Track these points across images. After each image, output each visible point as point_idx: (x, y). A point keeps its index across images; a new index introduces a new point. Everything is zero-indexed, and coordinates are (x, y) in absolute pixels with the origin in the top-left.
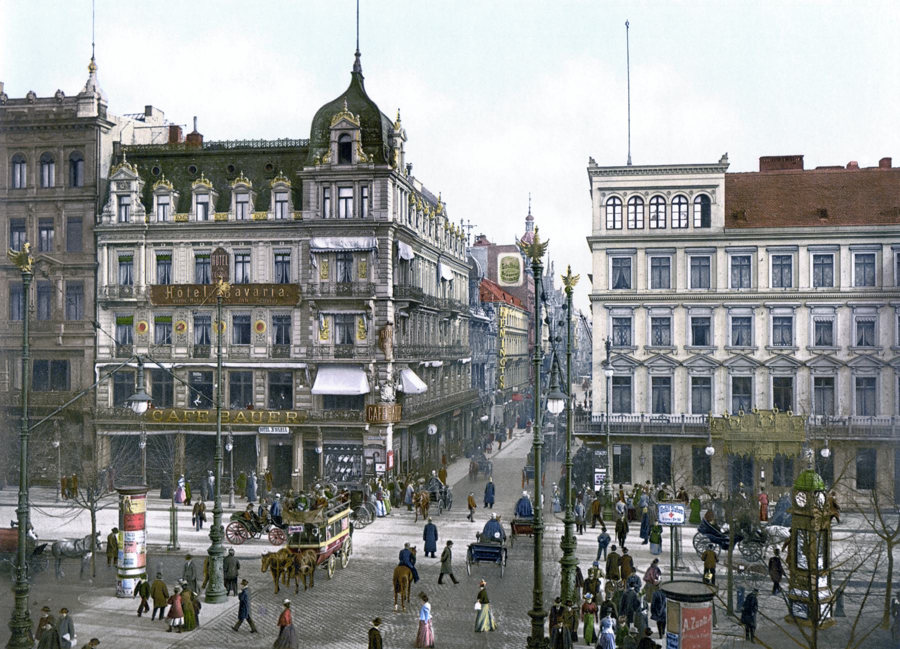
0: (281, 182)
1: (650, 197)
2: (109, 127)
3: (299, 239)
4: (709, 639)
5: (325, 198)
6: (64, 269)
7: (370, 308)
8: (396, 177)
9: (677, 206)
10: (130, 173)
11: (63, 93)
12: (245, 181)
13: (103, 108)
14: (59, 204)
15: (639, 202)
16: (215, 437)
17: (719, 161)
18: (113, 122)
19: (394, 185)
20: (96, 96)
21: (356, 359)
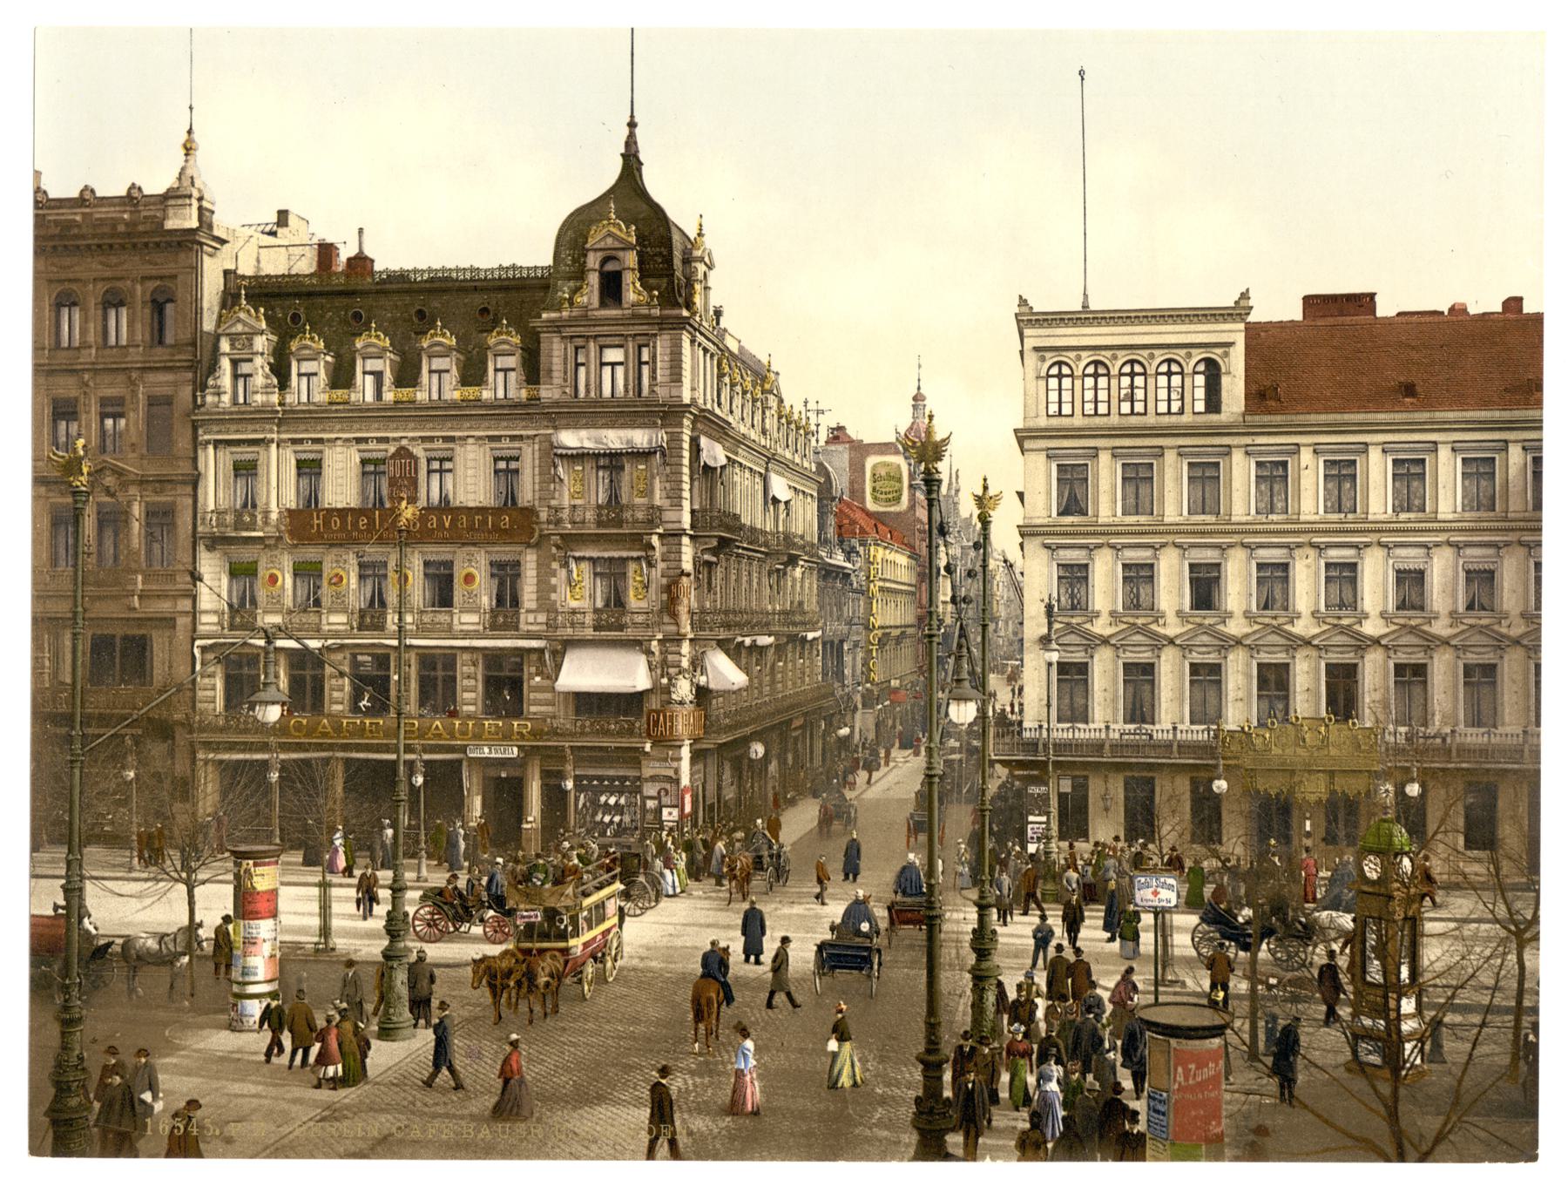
0: (504, 337)
2: (218, 246)
7: (654, 548)
8: (695, 329)
10: (252, 322)
11: (140, 189)
14: (134, 375)
15: (1101, 370)
16: (395, 763)
18: (224, 236)
19: (693, 342)
20: (196, 194)
21: (629, 633)
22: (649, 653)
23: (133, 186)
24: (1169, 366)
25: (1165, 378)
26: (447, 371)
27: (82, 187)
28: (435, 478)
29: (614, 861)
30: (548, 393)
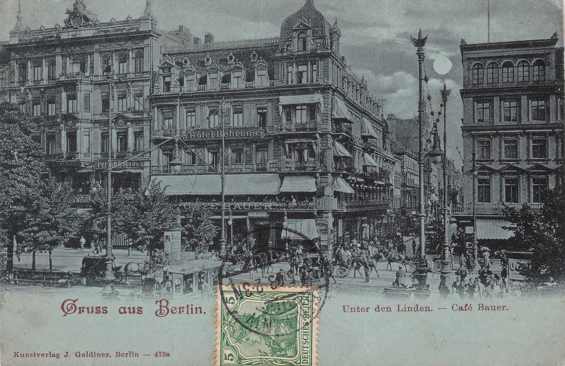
0: (261, 63)
1: (473, 64)
2: (158, 37)
3: (272, 98)
7: (317, 139)
8: (334, 58)
9: (522, 68)
10: (171, 63)
11: (115, 20)
13: (155, 26)
14: (129, 84)
15: (525, 64)
16: (221, 220)
17: (552, 37)
18: (160, 34)
19: (333, 63)
20: (150, 18)
21: (308, 170)
23: (57, 25)
24: (523, 63)
26: (264, 75)
30: (277, 83)
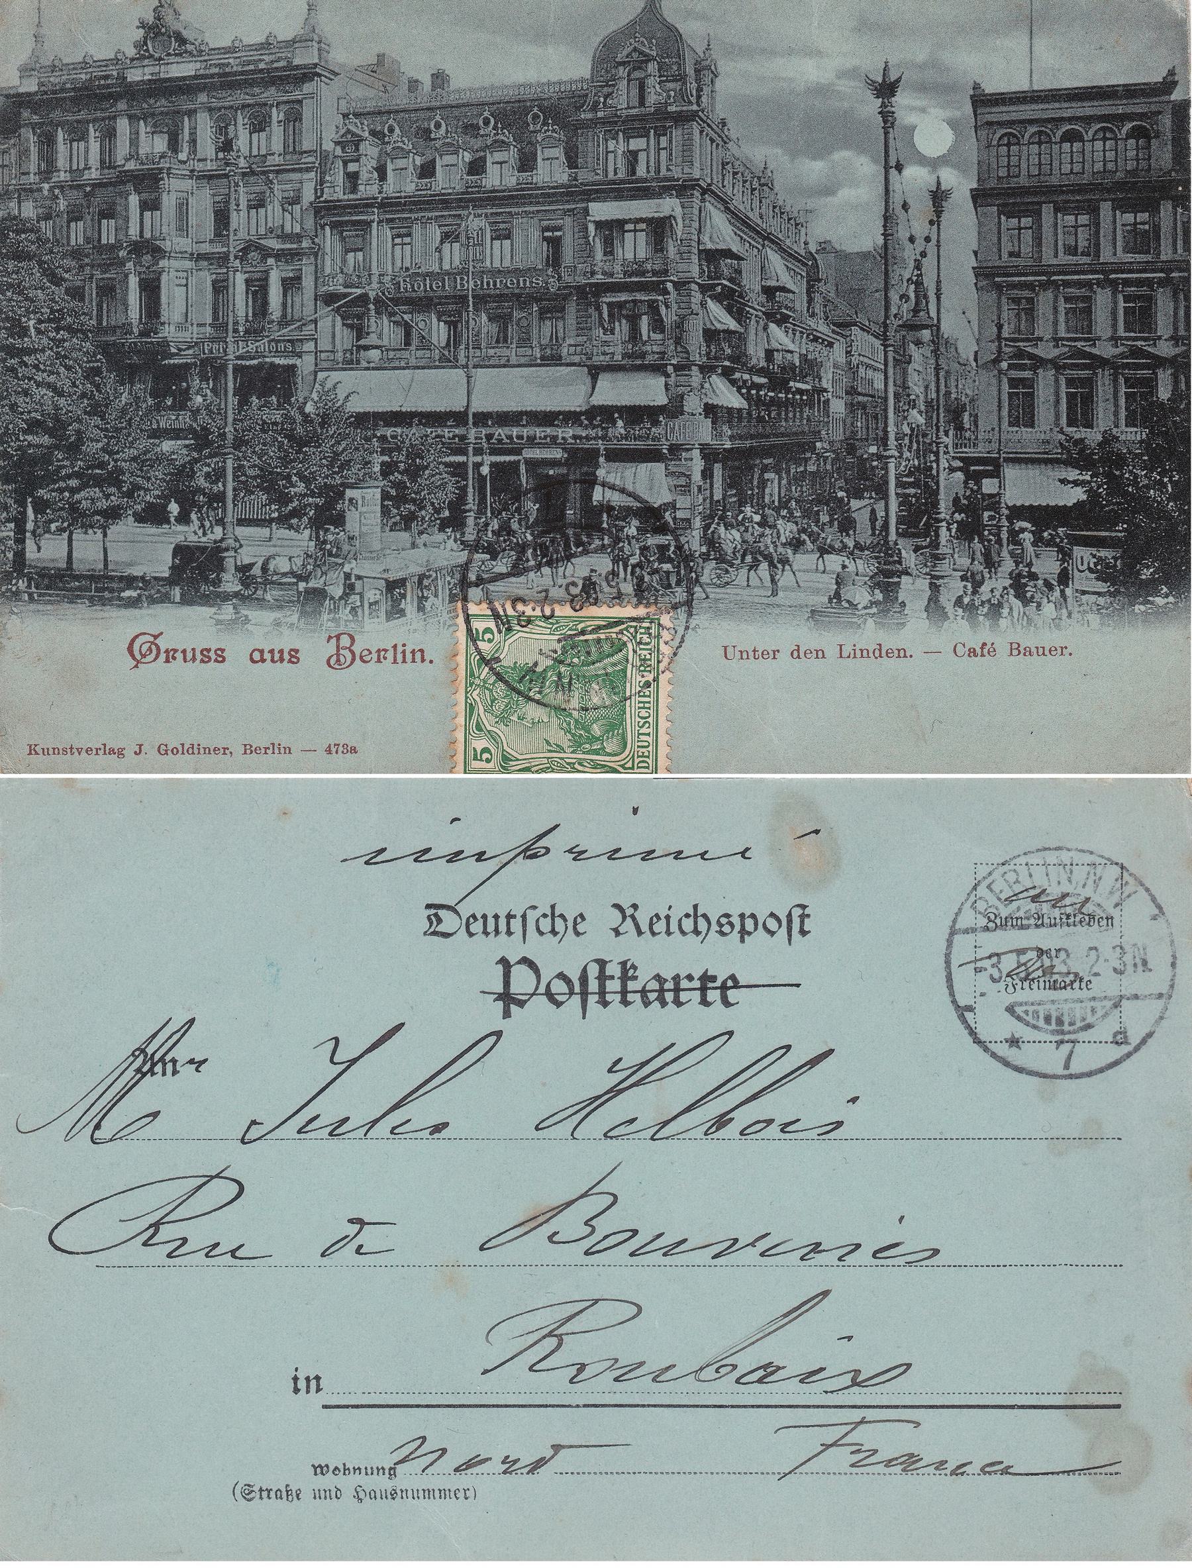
0: (550, 133)
1: (998, 136)
2: (332, 77)
4: (15, 533)
5: (608, 152)
6: (279, 255)
7: (669, 293)
10: (360, 133)
11: (241, 41)
12: (554, 131)
14: (271, 176)
16: (465, 464)
17: (1164, 78)
18: (337, 70)
20: (316, 38)
21: (649, 359)
22: (667, 376)
23: (119, 51)
25: (1005, 148)
27: (233, 38)
28: (398, 248)
29: (321, 549)
30: (584, 176)
